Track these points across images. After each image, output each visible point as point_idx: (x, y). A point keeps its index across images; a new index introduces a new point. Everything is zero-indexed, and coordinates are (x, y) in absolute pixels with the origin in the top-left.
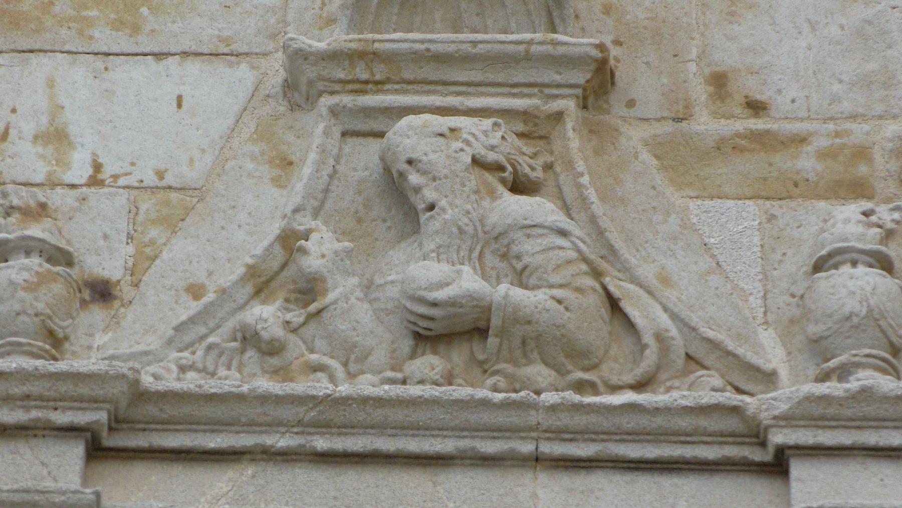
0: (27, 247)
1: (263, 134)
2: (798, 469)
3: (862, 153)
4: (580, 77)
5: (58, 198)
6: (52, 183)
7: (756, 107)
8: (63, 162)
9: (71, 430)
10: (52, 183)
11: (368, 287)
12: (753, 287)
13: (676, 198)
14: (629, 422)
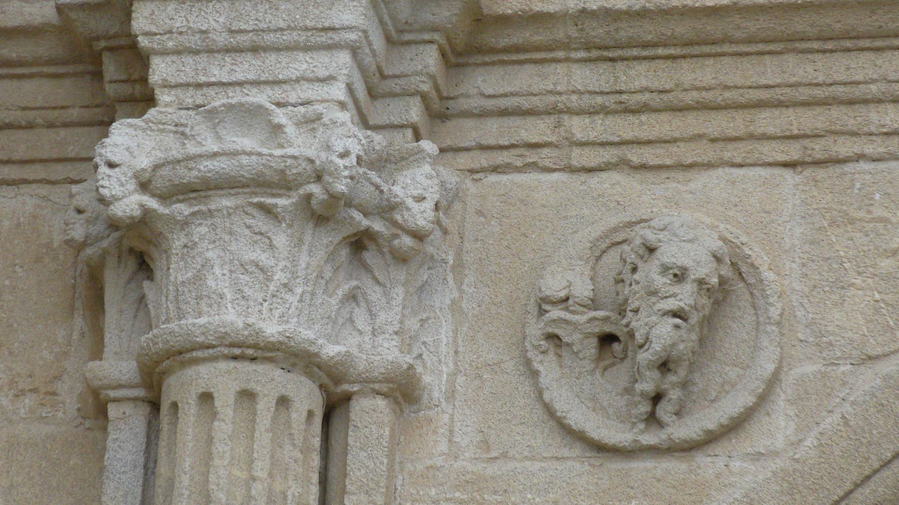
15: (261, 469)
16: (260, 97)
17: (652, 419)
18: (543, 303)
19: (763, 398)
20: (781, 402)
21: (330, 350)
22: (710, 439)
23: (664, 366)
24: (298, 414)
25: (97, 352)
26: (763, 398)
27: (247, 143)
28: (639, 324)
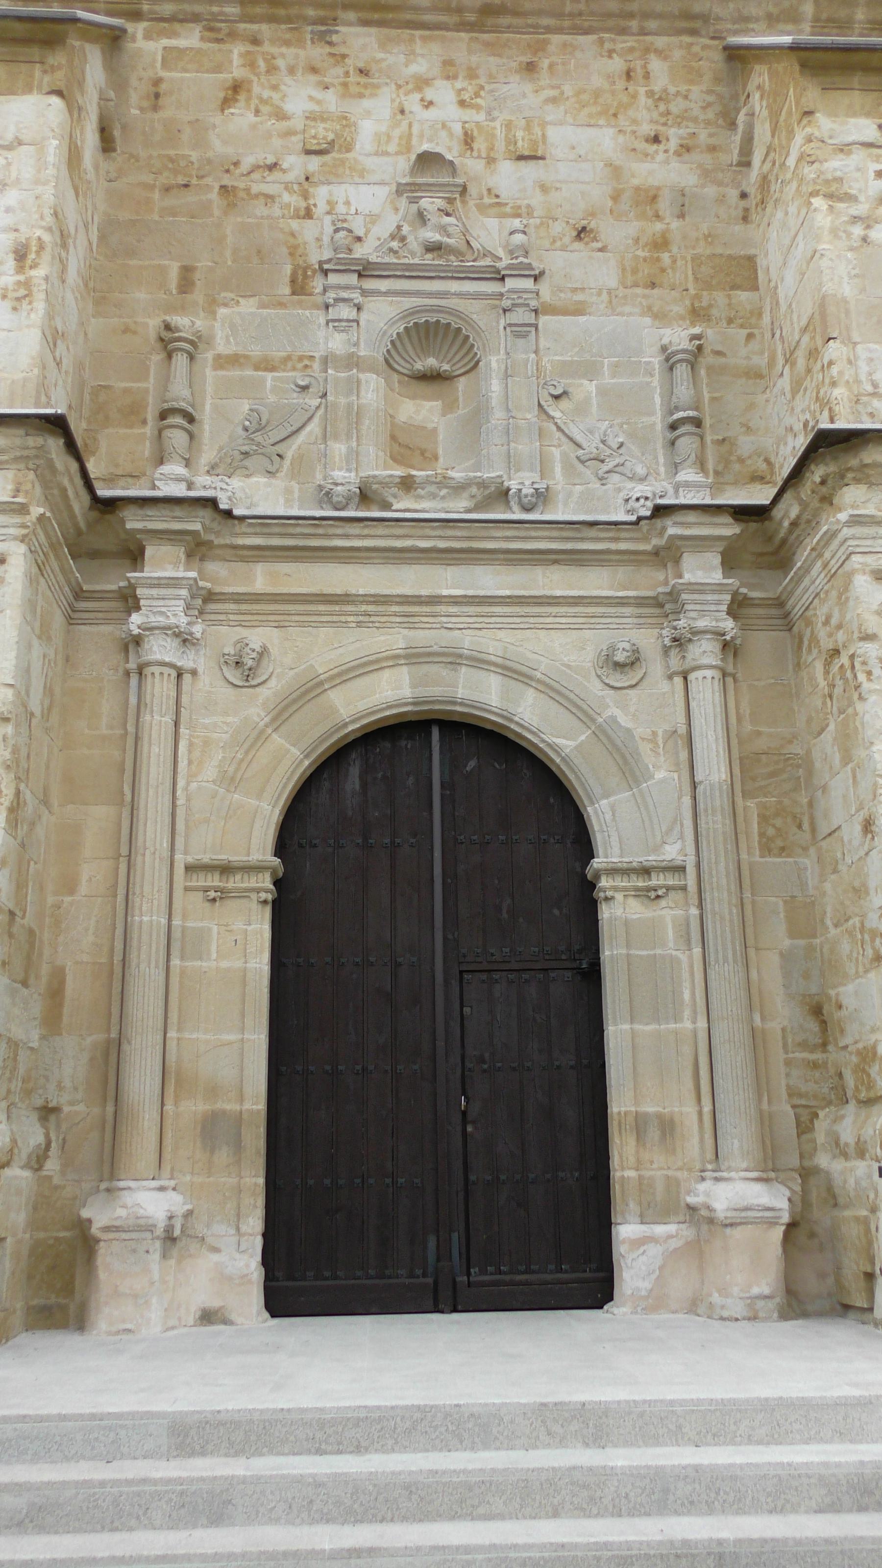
0: (343, 229)
1: (392, 202)
2: (507, 280)
3: (519, 207)
4: (460, 189)
5: (349, 217)
6: (347, 214)
7: (497, 196)
8: (349, 209)
9: (355, 271)
10: (347, 214)
11: (416, 238)
12: (496, 237)
13: (481, 217)
14: (472, 269)
15: (711, 824)
16: (163, 609)
17: (247, 680)
18: (224, 655)
19: (270, 676)
20: (274, 679)
21: (179, 664)
22: (259, 684)
23: (250, 669)
24: (172, 678)
25: (127, 662)
26: (270, 676)
27: (161, 619)
28: (245, 660)
